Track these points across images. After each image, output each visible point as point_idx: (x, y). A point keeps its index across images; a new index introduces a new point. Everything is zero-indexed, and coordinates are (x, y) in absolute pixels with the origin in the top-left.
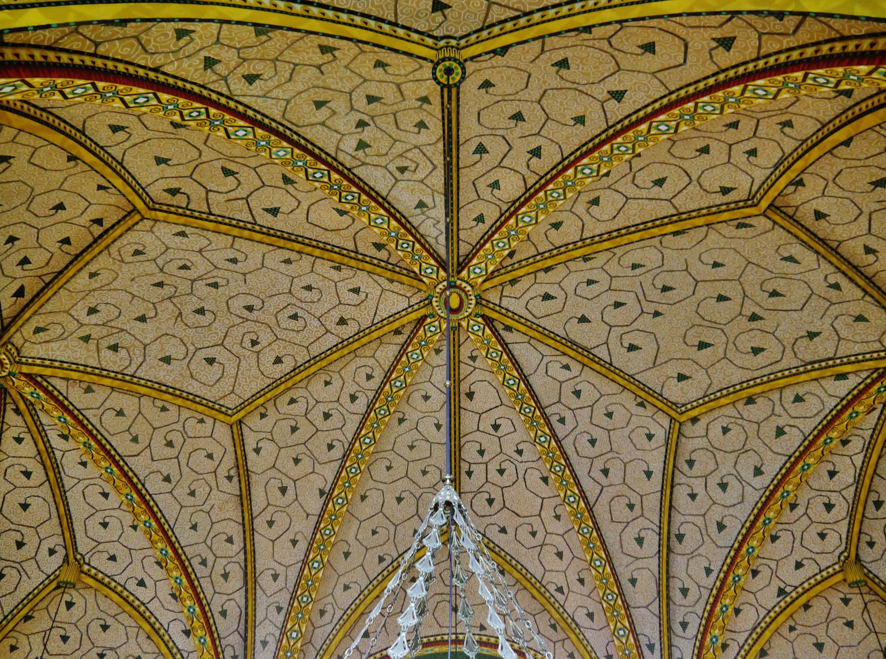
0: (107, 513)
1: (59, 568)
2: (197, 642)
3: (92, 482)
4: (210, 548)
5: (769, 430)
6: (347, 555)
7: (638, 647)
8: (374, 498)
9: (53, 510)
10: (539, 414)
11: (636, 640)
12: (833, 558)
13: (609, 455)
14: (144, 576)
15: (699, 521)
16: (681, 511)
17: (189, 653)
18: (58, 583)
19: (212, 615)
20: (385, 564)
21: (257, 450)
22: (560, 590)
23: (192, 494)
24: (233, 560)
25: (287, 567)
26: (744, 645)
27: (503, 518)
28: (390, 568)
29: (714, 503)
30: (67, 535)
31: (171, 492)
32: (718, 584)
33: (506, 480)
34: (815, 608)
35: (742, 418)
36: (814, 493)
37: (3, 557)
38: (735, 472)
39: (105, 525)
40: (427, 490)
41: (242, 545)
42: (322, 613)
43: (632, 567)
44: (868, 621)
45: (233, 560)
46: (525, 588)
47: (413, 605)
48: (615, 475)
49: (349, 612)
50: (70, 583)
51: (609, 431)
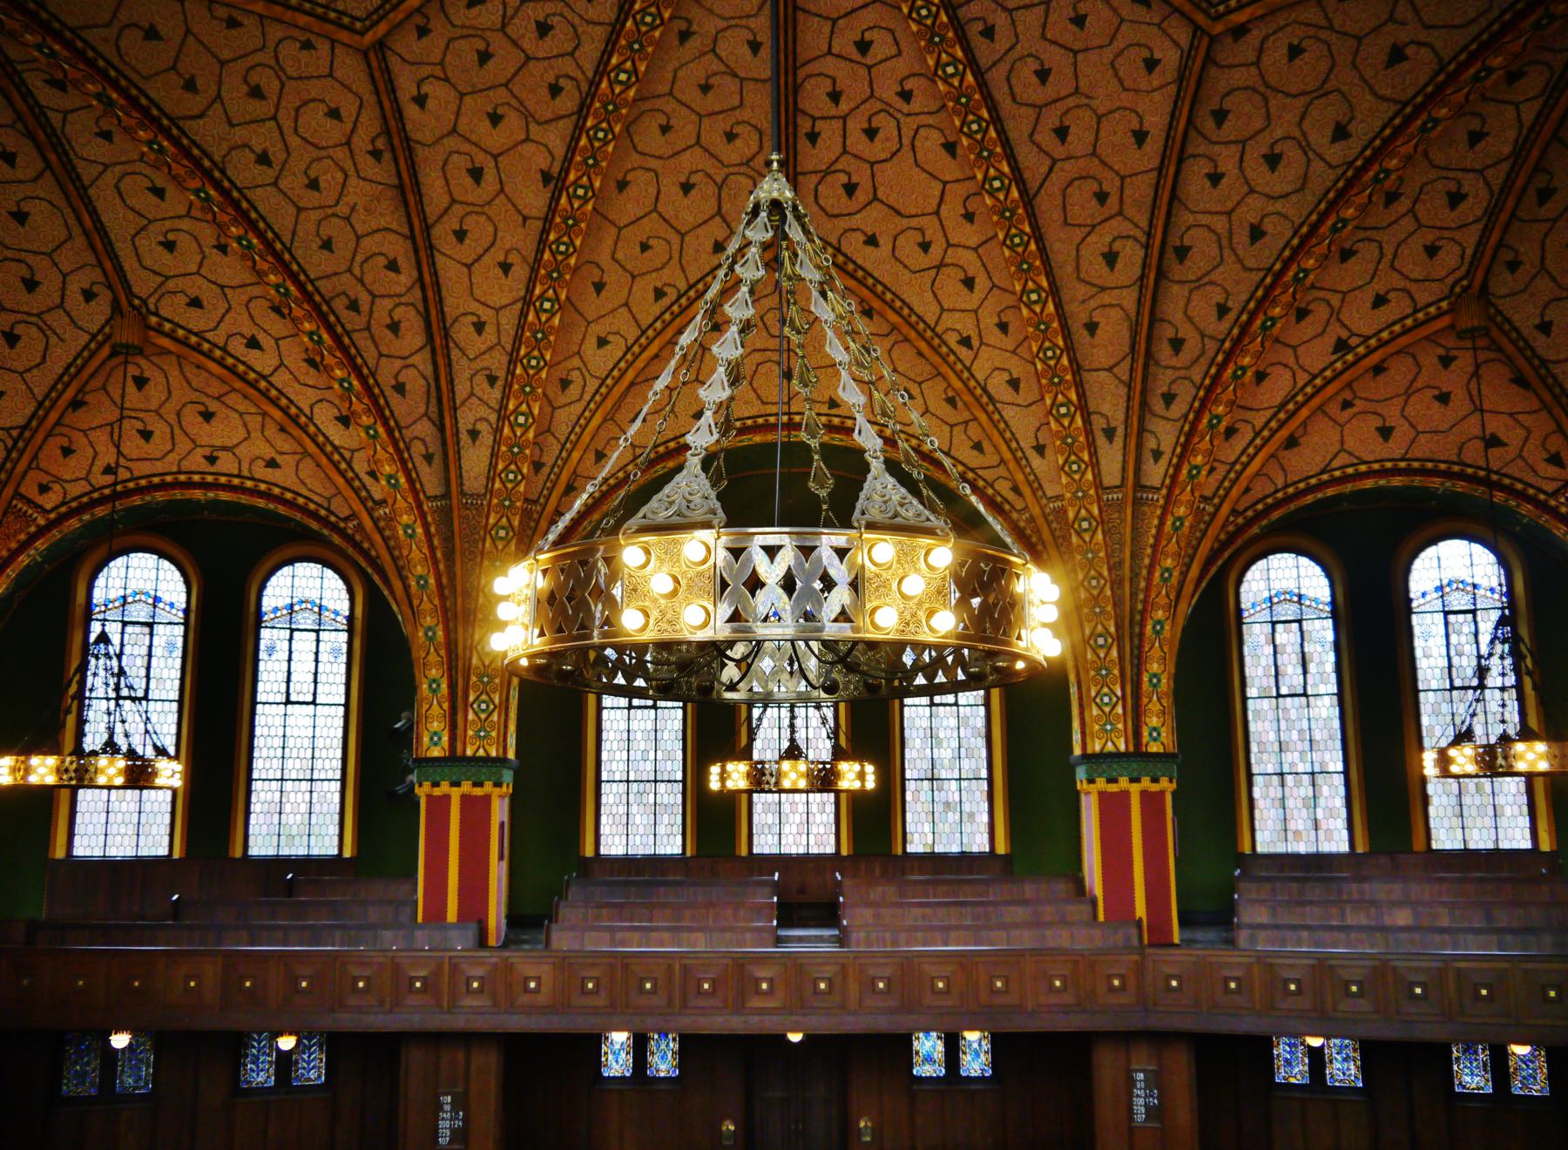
0: (168, 224)
1: (107, 322)
2: (363, 434)
3: (128, 168)
4: (361, 281)
5: (1376, 50)
6: (599, 287)
7: (1089, 432)
8: (642, 185)
9: (72, 221)
10: (945, 19)
11: (1087, 421)
12: (1437, 290)
13: (1071, 102)
14: (255, 331)
15: (1220, 223)
16: (1191, 206)
17: (353, 451)
18: (113, 347)
19: (382, 392)
20: (666, 301)
21: (421, 100)
22: (965, 342)
23: (314, 185)
24: (403, 300)
25: (497, 310)
26: (1263, 429)
27: (872, 219)
28: (675, 308)
29: (1252, 191)
30: (108, 265)
31: (275, 184)
32: (1236, 331)
33: (879, 149)
34: (1392, 372)
35: (1331, 28)
36: (1433, 174)
37: (8, 306)
38: (1297, 134)
39: (170, 246)
40: (736, 170)
41: (415, 274)
42: (565, 384)
43: (1093, 303)
44: (1475, 393)
45: (403, 300)
46: (907, 340)
47: (722, 369)
48: (1079, 138)
49: (609, 382)
50: (136, 347)
51: (1075, 53)
